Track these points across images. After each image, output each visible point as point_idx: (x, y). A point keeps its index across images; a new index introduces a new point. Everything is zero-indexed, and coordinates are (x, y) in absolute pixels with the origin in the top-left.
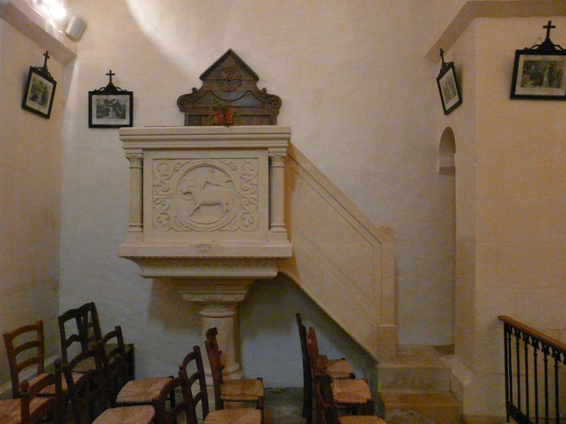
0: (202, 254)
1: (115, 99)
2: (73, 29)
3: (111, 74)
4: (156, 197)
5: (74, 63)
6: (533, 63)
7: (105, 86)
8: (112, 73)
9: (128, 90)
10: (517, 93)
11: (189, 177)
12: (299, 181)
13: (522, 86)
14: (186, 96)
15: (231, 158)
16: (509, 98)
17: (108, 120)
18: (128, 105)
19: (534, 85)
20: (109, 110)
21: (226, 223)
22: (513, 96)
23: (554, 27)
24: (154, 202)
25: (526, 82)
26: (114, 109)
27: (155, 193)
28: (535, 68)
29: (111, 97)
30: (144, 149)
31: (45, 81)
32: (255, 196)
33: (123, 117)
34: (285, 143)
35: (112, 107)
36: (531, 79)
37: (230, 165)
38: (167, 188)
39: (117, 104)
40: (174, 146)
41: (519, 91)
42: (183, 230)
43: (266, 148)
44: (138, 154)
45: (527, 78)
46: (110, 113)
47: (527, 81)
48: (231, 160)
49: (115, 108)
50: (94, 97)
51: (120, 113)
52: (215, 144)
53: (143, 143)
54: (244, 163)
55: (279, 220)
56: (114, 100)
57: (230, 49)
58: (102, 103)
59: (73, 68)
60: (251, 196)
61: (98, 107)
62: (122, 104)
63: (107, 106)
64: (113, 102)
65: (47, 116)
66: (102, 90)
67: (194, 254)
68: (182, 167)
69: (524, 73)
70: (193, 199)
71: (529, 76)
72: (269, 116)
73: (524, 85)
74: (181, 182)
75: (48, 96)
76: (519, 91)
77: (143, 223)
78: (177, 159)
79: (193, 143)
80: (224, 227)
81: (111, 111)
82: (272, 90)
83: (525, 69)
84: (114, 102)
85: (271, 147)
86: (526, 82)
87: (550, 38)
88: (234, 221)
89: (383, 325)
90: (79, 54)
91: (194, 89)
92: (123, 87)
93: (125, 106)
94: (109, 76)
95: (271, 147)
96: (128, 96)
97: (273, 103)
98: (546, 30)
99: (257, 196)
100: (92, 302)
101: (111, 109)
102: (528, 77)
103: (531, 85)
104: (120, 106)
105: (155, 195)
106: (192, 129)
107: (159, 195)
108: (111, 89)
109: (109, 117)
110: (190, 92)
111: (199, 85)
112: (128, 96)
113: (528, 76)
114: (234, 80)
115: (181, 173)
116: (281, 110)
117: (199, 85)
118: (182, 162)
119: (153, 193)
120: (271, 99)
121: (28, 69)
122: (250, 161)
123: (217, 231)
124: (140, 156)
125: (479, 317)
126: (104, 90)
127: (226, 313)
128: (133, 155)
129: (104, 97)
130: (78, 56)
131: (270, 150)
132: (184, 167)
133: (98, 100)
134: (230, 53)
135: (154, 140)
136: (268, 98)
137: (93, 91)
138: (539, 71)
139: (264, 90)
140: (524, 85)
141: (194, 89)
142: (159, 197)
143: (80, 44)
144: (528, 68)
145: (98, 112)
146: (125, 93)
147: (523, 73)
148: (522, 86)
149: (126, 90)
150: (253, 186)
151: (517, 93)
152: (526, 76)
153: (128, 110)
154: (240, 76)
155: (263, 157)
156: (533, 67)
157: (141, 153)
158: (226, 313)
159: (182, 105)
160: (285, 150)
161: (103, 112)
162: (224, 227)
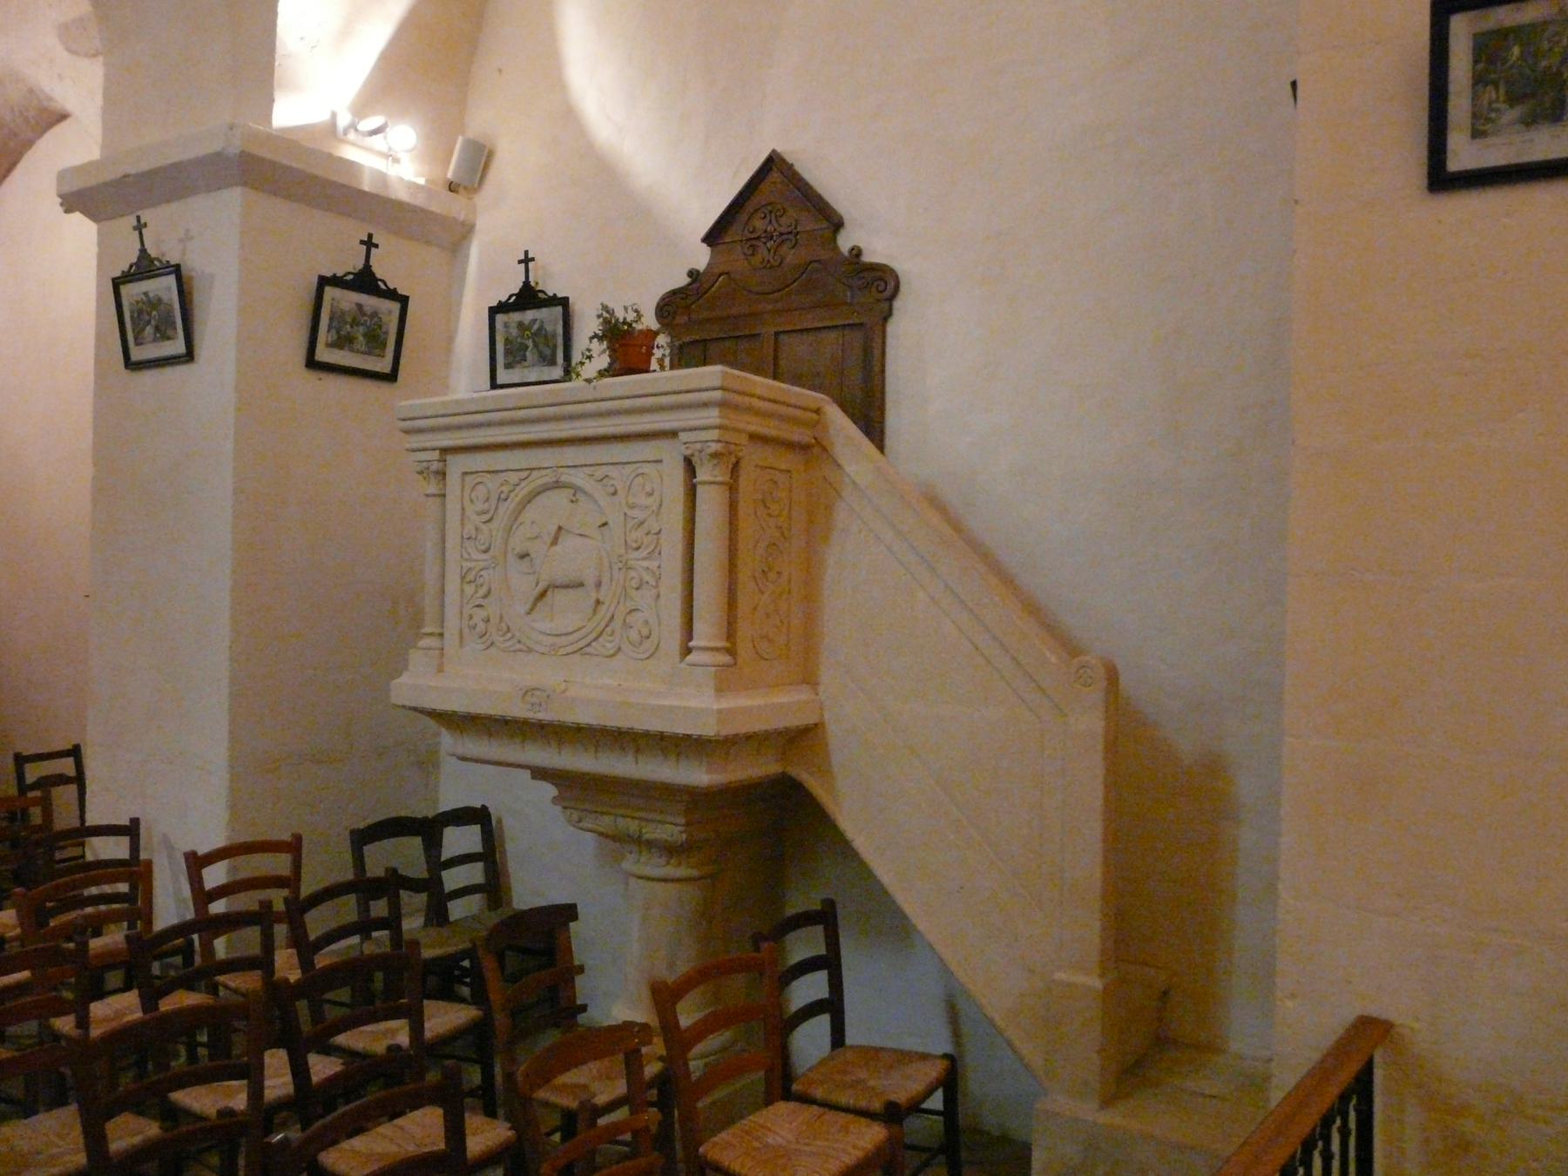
0: (535, 713)
1: (536, 320)
2: (455, 172)
3: (526, 260)
4: (467, 565)
5: (468, 248)
6: (1512, 36)
7: (517, 291)
8: (374, 241)
9: (560, 295)
10: (1454, 165)
11: (529, 515)
12: (841, 516)
13: (1477, 134)
14: (674, 293)
15: (512, 470)
16: (1426, 190)
17: (526, 371)
18: (560, 330)
19: (1530, 121)
20: (527, 347)
21: (594, 635)
22: (1441, 179)
23: (376, 246)
24: (463, 578)
25: (1493, 115)
26: (534, 341)
27: (466, 556)
28: (1522, 57)
29: (529, 315)
30: (445, 451)
31: (370, 302)
32: (653, 564)
33: (553, 363)
34: (713, 417)
35: (530, 340)
36: (1513, 100)
37: (605, 481)
38: (487, 545)
39: (541, 328)
40: (545, 436)
41: (1463, 154)
42: (512, 649)
43: (673, 434)
44: (709, 444)
45: (1497, 100)
46: (528, 353)
47: (1497, 110)
48: (605, 468)
49: (536, 339)
50: (330, 292)
51: (548, 352)
52: (652, 422)
53: (439, 436)
54: (634, 474)
55: (707, 631)
56: (534, 321)
57: (774, 151)
58: (514, 332)
59: (467, 256)
60: (645, 564)
61: (507, 341)
62: (549, 328)
63: (523, 337)
64: (532, 327)
65: (391, 377)
66: (351, 277)
67: (519, 711)
68: (514, 490)
69: (1479, 80)
70: (534, 573)
71: (1502, 91)
72: (862, 324)
73: (1486, 127)
74: (514, 527)
75: (386, 333)
76: (1463, 154)
77: (443, 627)
78: (502, 471)
79: (520, 429)
80: (589, 645)
81: (530, 348)
82: (875, 253)
83: (1480, 66)
84: (536, 327)
85: (684, 430)
86: (1493, 115)
87: (371, 264)
88: (609, 630)
89: (1061, 976)
90: (481, 224)
91: (693, 274)
92: (552, 288)
93: (554, 336)
94: (523, 265)
95: (684, 430)
96: (559, 309)
97: (874, 289)
98: (523, 265)
99: (656, 564)
100: (483, 806)
101: (530, 343)
102: (1498, 98)
103: (1512, 123)
104: (546, 336)
105: (467, 560)
106: (506, 396)
107: (470, 560)
108: (528, 297)
109: (526, 364)
110: (683, 281)
111: (701, 257)
112: (559, 309)
113: (1497, 92)
114: (782, 234)
115: (510, 505)
116: (898, 304)
117: (701, 257)
118: (513, 478)
119: (462, 556)
120: (869, 276)
121: (316, 280)
122: (646, 469)
123: (577, 656)
124: (435, 466)
125: (1290, 1004)
126: (515, 300)
127: (683, 872)
128: (698, 446)
129: (516, 317)
130: (478, 227)
131: (683, 436)
132: (518, 489)
133: (506, 325)
134: (773, 164)
135: (459, 427)
136: (861, 275)
137: (496, 305)
138: (1544, 63)
139: (857, 252)
140: (1486, 127)
141: (693, 274)
142: (472, 564)
143: (483, 199)
144: (1491, 61)
145: (508, 352)
146: (392, 294)
147: (1475, 84)
148: (1477, 134)
149: (555, 295)
150: (650, 537)
151: (1454, 165)
152: (1490, 93)
153: (560, 340)
154: (794, 223)
155: (670, 455)
156: (1516, 51)
157: (439, 461)
158: (683, 872)
159: (669, 314)
160: (714, 434)
161: (516, 355)
162: (589, 645)
